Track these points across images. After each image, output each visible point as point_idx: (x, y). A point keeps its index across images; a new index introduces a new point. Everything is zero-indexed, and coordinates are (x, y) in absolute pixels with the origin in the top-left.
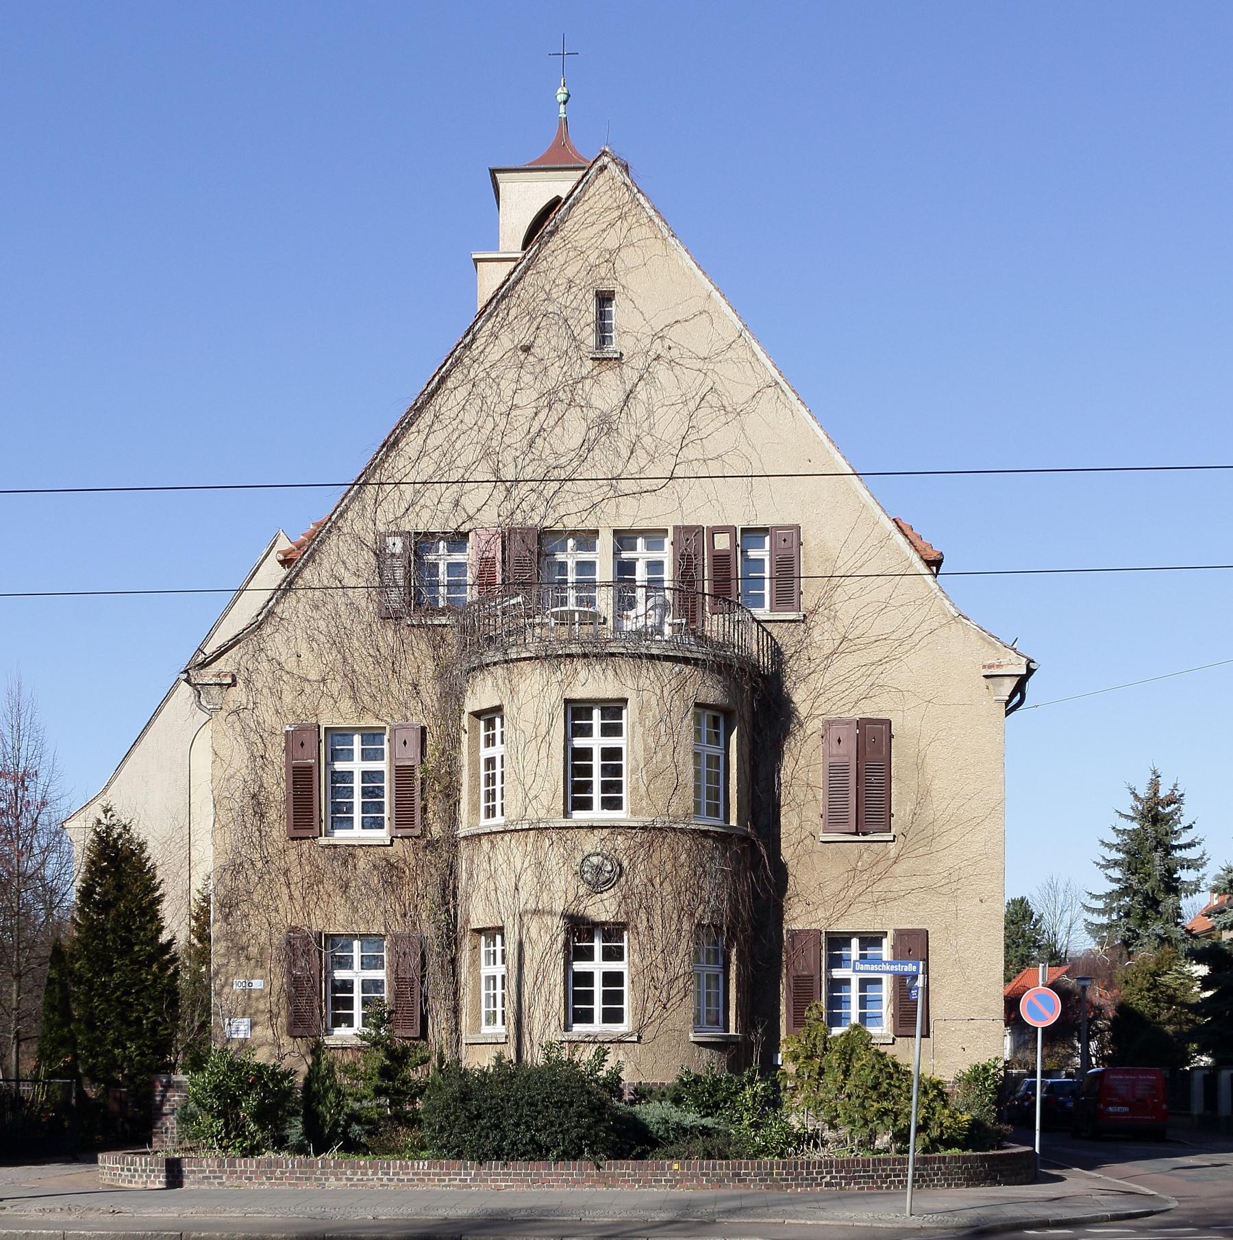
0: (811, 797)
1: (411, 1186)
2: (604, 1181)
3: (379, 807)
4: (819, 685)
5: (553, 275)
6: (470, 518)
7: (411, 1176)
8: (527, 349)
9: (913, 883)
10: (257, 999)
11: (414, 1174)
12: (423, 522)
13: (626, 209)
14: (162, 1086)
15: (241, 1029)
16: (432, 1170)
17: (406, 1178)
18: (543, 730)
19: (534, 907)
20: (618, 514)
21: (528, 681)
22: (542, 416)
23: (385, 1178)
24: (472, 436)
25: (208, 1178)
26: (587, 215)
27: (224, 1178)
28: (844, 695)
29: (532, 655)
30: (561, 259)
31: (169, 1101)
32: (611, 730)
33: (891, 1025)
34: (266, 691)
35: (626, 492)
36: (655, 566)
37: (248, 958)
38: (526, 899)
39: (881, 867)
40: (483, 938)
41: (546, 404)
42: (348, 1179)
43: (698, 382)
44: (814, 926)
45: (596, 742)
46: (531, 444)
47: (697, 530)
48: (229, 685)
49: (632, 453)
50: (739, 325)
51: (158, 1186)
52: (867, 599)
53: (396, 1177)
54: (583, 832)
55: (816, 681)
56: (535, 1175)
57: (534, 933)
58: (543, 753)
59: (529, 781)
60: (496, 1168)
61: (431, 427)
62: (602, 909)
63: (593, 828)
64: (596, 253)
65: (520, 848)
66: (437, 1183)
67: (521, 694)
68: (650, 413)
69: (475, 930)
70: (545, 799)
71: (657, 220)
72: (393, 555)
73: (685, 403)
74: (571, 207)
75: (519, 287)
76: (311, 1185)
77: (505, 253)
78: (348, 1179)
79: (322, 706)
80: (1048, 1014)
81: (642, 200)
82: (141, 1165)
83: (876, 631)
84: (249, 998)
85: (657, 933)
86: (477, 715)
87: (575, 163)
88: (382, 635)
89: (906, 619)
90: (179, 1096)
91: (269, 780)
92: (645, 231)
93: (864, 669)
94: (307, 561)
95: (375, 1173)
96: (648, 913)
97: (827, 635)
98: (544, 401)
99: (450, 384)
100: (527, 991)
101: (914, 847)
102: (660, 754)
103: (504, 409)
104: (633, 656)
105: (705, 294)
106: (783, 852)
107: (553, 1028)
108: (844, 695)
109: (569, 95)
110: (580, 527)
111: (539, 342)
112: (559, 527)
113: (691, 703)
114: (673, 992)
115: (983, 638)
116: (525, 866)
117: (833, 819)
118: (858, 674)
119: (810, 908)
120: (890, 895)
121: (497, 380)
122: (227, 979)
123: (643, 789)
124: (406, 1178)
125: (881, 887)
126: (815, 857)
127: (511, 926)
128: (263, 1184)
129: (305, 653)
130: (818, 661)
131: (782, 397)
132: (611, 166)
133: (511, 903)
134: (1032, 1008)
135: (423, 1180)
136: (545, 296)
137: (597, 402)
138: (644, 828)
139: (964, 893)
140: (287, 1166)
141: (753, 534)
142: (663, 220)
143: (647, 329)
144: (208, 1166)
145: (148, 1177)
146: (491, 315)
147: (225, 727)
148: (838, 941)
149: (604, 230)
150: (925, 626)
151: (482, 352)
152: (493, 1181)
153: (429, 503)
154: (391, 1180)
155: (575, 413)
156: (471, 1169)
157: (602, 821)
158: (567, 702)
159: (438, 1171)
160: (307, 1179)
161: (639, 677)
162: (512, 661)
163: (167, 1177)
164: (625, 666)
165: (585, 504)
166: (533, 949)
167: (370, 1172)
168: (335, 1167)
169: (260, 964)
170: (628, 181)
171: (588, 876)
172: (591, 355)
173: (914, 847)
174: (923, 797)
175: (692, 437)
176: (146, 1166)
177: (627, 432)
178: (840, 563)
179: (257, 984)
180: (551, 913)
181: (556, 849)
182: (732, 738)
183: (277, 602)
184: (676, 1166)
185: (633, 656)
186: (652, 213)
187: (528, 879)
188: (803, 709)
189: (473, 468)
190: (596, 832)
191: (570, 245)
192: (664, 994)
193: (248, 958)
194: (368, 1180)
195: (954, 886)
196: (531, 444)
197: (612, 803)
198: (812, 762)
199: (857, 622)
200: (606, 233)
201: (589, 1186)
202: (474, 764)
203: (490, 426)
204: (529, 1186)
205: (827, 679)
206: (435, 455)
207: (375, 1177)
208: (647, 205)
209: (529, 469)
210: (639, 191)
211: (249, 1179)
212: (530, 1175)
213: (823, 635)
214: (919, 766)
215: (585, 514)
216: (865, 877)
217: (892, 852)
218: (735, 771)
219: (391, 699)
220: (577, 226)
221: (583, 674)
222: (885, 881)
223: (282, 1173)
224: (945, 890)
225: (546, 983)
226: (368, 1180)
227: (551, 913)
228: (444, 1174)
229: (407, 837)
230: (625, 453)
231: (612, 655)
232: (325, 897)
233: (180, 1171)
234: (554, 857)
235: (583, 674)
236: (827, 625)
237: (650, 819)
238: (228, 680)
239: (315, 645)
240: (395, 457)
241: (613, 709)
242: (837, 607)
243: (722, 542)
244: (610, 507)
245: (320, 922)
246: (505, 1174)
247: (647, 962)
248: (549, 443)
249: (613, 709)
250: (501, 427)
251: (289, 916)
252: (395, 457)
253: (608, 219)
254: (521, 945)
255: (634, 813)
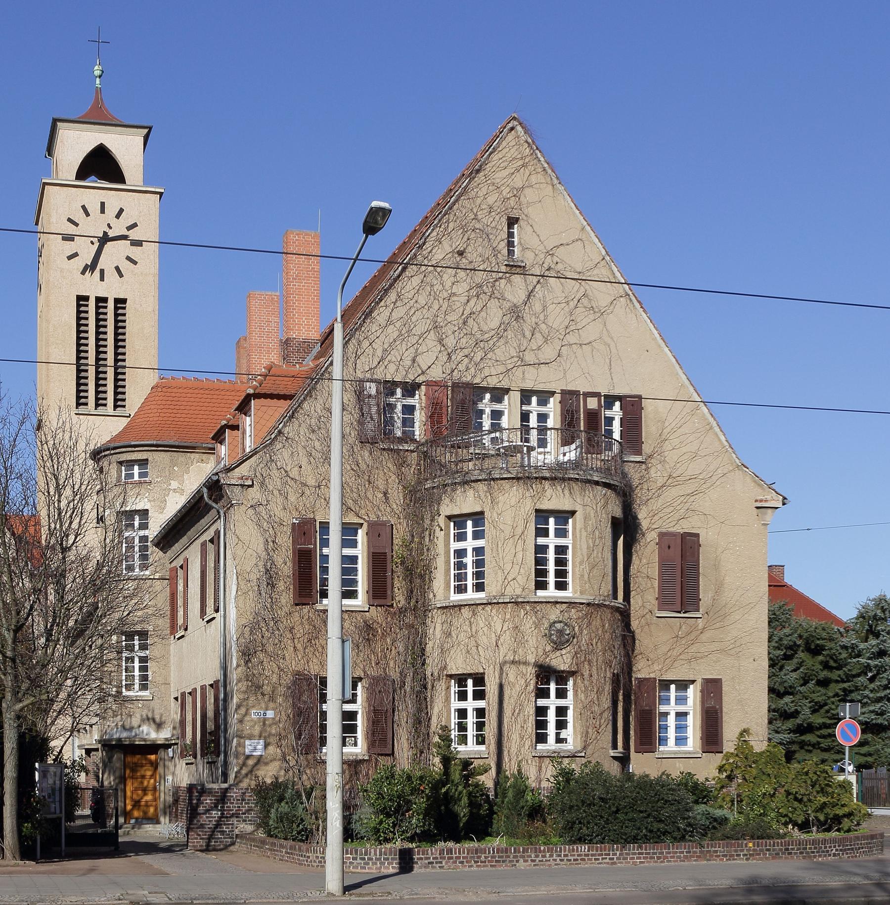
0: (649, 585)
1: (576, 864)
2: (702, 856)
3: (354, 582)
4: (654, 508)
5: (479, 201)
6: (423, 373)
7: (576, 857)
8: (461, 253)
9: (714, 646)
10: (270, 726)
11: (578, 855)
12: (391, 373)
13: (527, 160)
14: (197, 792)
15: (254, 747)
16: (591, 852)
17: (572, 858)
18: (519, 531)
19: (512, 659)
20: (524, 379)
21: (507, 495)
22: (472, 302)
23: (558, 859)
24: (424, 313)
25: (432, 863)
26: (501, 161)
27: (444, 863)
28: (669, 516)
29: (512, 476)
30: (484, 190)
31: (203, 803)
32: (561, 533)
33: (699, 743)
34: (276, 492)
35: (530, 363)
36: (542, 417)
37: (263, 694)
38: (505, 653)
39: (693, 636)
40: (453, 681)
41: (474, 294)
42: (533, 861)
43: (576, 289)
44: (652, 676)
45: (552, 541)
46: (465, 323)
47: (576, 393)
48: (249, 486)
49: (533, 335)
50: (604, 252)
51: (391, 871)
52: (684, 450)
53: (566, 858)
54: (549, 605)
55: (655, 505)
56: (660, 853)
57: (512, 677)
58: (519, 548)
59: (508, 567)
60: (634, 849)
61: (395, 303)
62: (562, 661)
63: (557, 603)
64: (508, 189)
65: (500, 616)
66: (593, 861)
67: (500, 505)
68: (545, 308)
69: (447, 675)
70: (521, 580)
71: (549, 171)
72: (370, 396)
73: (567, 303)
74: (490, 154)
75: (455, 207)
76: (506, 866)
77: (61, 180)
78: (533, 861)
79: (318, 505)
80: (853, 737)
81: (539, 155)
82: (375, 854)
83: (689, 472)
84: (264, 724)
85: (595, 676)
86: (450, 518)
87: (105, 120)
88: (361, 455)
89: (708, 465)
90: (211, 800)
91: (279, 561)
92: (540, 178)
93: (682, 498)
94: (307, 395)
95: (551, 856)
96: (590, 664)
97: (659, 474)
98: (474, 292)
99: (407, 273)
100: (506, 721)
101: (714, 622)
102: (595, 552)
103: (446, 295)
104: (582, 481)
105: (579, 227)
106: (632, 623)
107: (527, 747)
108: (669, 516)
109: (103, 72)
110: (498, 386)
111: (469, 249)
112: (484, 384)
113: (610, 517)
114: (603, 721)
115: (755, 482)
116: (504, 629)
117: (664, 602)
118: (679, 502)
119: (650, 663)
120: (699, 655)
121: (441, 274)
122: (247, 710)
123: (586, 576)
124: (572, 858)
125: (693, 649)
126: (653, 627)
127: (492, 672)
128: (472, 866)
129: (304, 463)
130: (653, 491)
131: (631, 306)
132: (519, 128)
133: (492, 656)
134: (843, 733)
135: (584, 860)
136: (473, 216)
137: (508, 296)
138: (588, 604)
139: (743, 655)
140: (489, 853)
141: (610, 400)
142: (553, 171)
143: (541, 248)
144: (432, 854)
145: (381, 863)
146: (436, 226)
147: (245, 518)
148: (665, 685)
149: (513, 174)
150: (719, 471)
151: (431, 252)
152: (638, 858)
153: (394, 359)
154: (561, 860)
155: (493, 303)
156: (617, 851)
157: (561, 598)
158: (537, 511)
159: (594, 853)
160: (503, 861)
161: (584, 496)
162: (493, 479)
163: (400, 863)
164: (576, 487)
165: (501, 369)
166: (512, 689)
167: (548, 855)
168: (523, 852)
169: (272, 699)
170: (530, 140)
171: (554, 637)
172: (506, 263)
173: (714, 622)
174: (719, 588)
175: (572, 328)
176: (381, 855)
177: (530, 320)
178: (667, 424)
179: (270, 714)
180: (525, 663)
181: (529, 617)
182: (619, 542)
183: (285, 426)
184: (751, 845)
185: (582, 481)
186: (546, 165)
187: (506, 638)
188: (645, 524)
189: (424, 336)
190: (558, 606)
191: (488, 182)
192: (598, 722)
193: (263, 694)
194: (546, 861)
195: (738, 650)
196: (465, 323)
197: (479, 587)
198: (651, 561)
199: (678, 465)
200: (514, 176)
201: (695, 861)
202: (447, 552)
203: (436, 307)
204: (656, 862)
205: (659, 504)
206: (398, 324)
207: (551, 859)
208: (542, 159)
209: (464, 341)
210: (537, 149)
211: (462, 862)
212: (655, 853)
213: (657, 474)
214: (716, 567)
215: (501, 377)
216: (683, 642)
217: (700, 625)
218: (622, 566)
219: (367, 502)
220: (494, 168)
221: (549, 492)
222: (696, 645)
223: (486, 857)
224: (732, 652)
225: (521, 715)
226: (546, 861)
227: (525, 663)
228: (599, 855)
229: (380, 606)
230: (528, 334)
231: (570, 479)
232: (320, 649)
233: (412, 859)
234: (528, 624)
235: (549, 492)
236: (659, 467)
237: (592, 598)
238: (249, 483)
239: (312, 460)
240: (370, 323)
241: (563, 516)
242: (666, 454)
243: (592, 403)
244: (518, 372)
245: (316, 667)
246: (639, 854)
247: (589, 699)
248: (477, 322)
249: (563, 516)
250: (444, 308)
251: (294, 662)
252: (370, 323)
253: (515, 165)
254: (501, 687)
255: (575, 592)
